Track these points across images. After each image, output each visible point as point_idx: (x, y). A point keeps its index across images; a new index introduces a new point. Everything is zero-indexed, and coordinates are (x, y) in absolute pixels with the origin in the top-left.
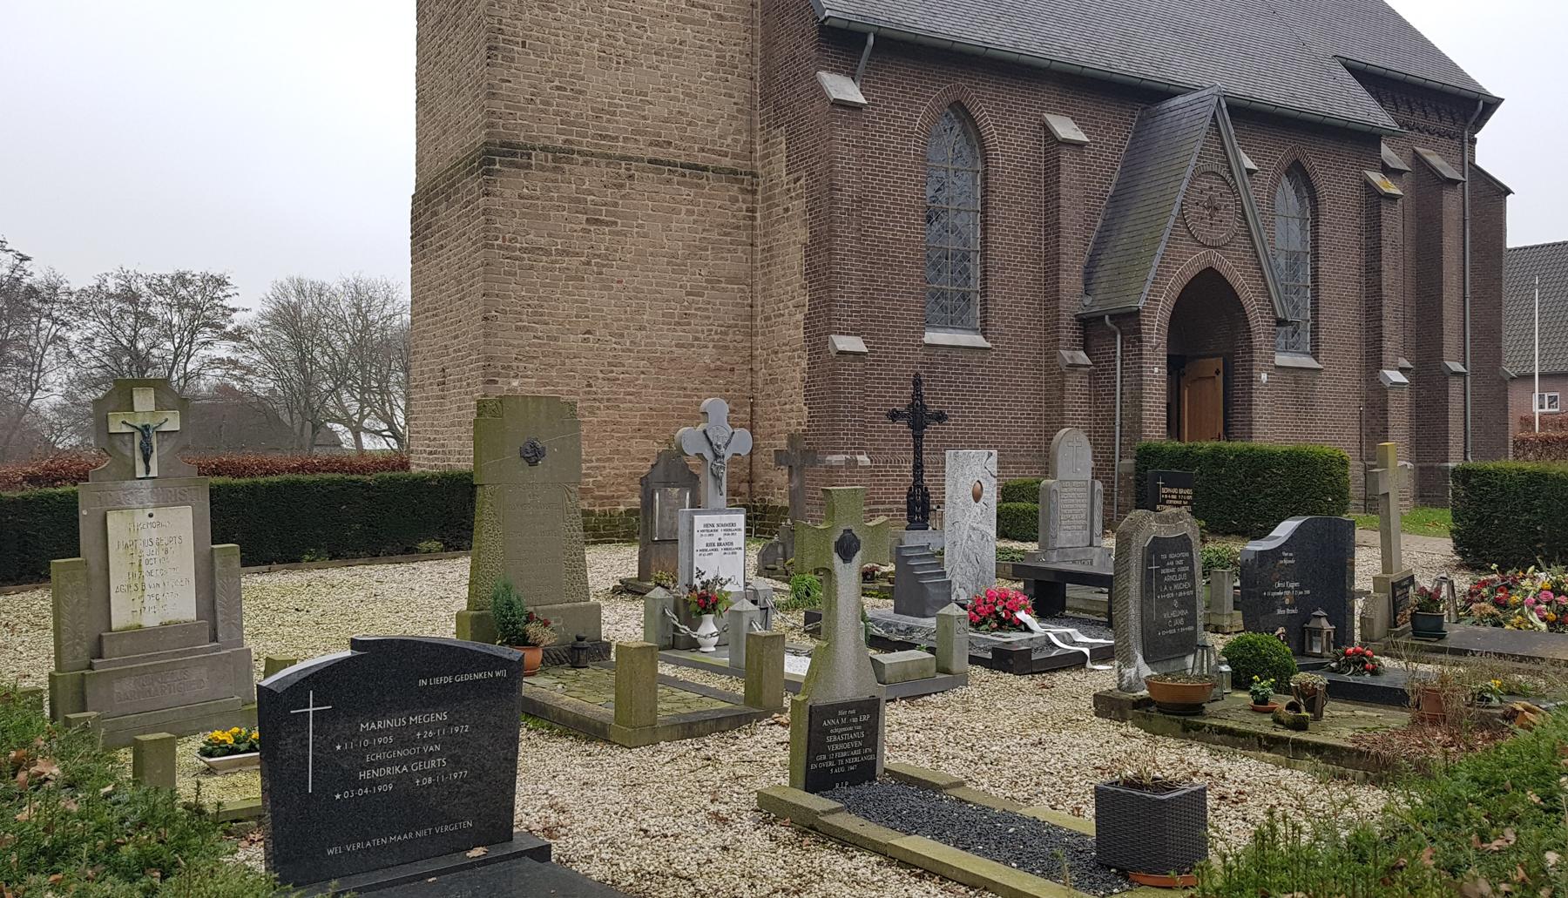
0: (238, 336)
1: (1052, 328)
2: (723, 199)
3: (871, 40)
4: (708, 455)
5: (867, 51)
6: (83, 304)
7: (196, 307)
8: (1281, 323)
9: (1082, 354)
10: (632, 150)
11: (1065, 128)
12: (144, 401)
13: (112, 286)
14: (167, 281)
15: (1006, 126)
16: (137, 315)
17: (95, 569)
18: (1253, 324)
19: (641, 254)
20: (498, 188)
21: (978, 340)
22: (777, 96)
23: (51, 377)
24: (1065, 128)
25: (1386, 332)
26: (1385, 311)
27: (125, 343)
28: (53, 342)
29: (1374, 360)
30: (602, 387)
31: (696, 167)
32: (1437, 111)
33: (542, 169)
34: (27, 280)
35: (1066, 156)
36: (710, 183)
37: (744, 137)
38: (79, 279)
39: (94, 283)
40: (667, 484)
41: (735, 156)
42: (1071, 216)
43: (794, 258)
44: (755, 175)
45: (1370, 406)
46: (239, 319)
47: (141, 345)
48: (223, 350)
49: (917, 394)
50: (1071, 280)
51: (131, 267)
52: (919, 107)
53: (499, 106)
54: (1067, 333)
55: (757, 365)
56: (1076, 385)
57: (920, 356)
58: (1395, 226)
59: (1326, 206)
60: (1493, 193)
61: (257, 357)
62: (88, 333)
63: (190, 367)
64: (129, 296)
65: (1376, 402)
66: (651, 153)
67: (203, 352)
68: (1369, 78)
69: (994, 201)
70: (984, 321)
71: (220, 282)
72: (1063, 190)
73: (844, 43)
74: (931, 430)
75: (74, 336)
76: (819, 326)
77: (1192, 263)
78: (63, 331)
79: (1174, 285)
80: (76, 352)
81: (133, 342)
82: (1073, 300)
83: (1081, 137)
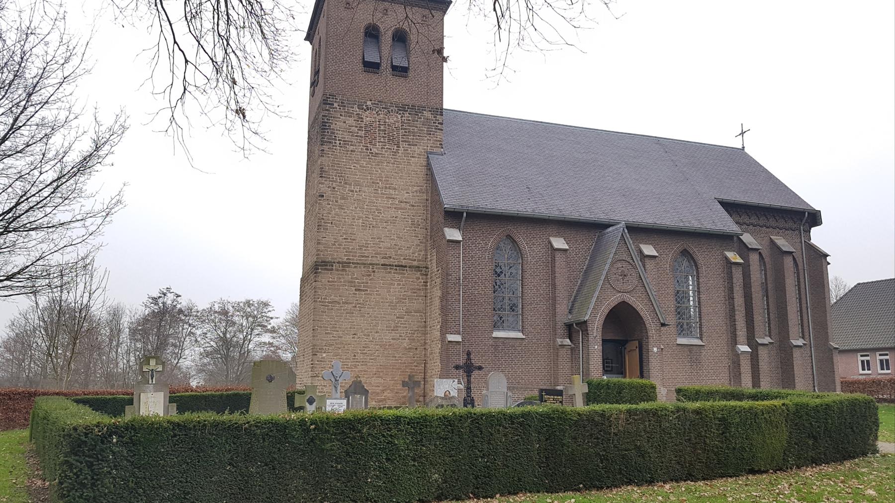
0: (273, 331)
1: (555, 329)
2: (413, 279)
3: (465, 214)
4: (333, 380)
5: (464, 219)
6: (204, 317)
7: (255, 317)
8: (663, 325)
9: (568, 340)
10: (375, 261)
11: (559, 243)
12: (153, 362)
13: (216, 308)
14: (241, 305)
15: (531, 245)
16: (227, 321)
17: (137, 409)
18: (648, 326)
19: (378, 302)
20: (319, 279)
21: (520, 335)
22: (434, 237)
23: (187, 352)
24: (559, 243)
25: (738, 327)
26: (737, 317)
27: (221, 335)
28: (189, 335)
29: (734, 342)
30: (360, 357)
31: (402, 266)
32: (783, 217)
33: (337, 270)
34: (179, 306)
35: (558, 255)
36: (408, 272)
37: (423, 253)
38: (202, 305)
39: (209, 306)
40: (355, 393)
41: (419, 261)
42: (561, 280)
43: (437, 302)
44: (427, 268)
45: (734, 363)
46: (274, 323)
47: (228, 336)
48: (266, 338)
49: (469, 359)
50: (562, 308)
51: (225, 298)
52: (489, 240)
53: (321, 247)
54: (561, 330)
55: (427, 347)
56: (564, 354)
57: (491, 342)
58: (738, 274)
59: (703, 269)
60: (819, 258)
61: (283, 341)
62: (205, 331)
63: (250, 346)
64: (224, 312)
65: (736, 359)
66: (382, 261)
67: (257, 339)
68: (730, 207)
69: (527, 275)
70: (701, 335)
71: (266, 304)
73: (454, 217)
74: (475, 373)
75: (199, 332)
76: (444, 331)
77: (613, 300)
78: (194, 330)
79: (604, 310)
80: (199, 339)
81: (225, 334)
82: (563, 315)
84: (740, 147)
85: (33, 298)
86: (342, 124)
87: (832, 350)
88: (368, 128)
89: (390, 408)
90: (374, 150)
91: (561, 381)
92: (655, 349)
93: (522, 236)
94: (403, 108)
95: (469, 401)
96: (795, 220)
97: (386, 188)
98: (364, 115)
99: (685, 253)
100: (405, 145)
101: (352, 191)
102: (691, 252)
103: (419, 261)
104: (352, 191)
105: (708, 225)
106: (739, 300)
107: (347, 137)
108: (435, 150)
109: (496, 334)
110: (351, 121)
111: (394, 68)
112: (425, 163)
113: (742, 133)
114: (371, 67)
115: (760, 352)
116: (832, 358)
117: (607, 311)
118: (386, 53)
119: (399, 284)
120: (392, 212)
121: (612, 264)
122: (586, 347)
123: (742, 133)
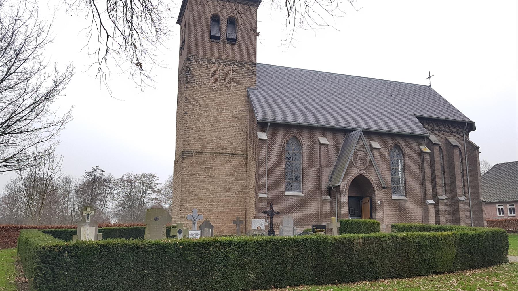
0: (158, 191)
1: (321, 191)
2: (239, 161)
3: (269, 124)
4: (193, 220)
5: (268, 127)
6: (118, 183)
7: (147, 183)
8: (384, 188)
9: (329, 197)
10: (217, 151)
11: (323, 141)
12: (88, 210)
13: (125, 178)
14: (140, 176)
15: (307, 142)
16: (131, 186)
17: (79, 236)
18: (375, 188)
20: (185, 161)
21: (301, 194)
22: (251, 137)
23: (108, 204)
24: (323, 141)
25: (427, 189)
26: (426, 183)
27: (128, 194)
28: (109, 194)
29: (425, 198)
30: (208, 206)
31: (233, 154)
33: (195, 156)
34: (103, 177)
35: (323, 148)
36: (236, 158)
37: (245, 146)
38: (117, 176)
39: (121, 177)
40: (206, 228)
41: (242, 151)
42: (325, 162)
43: (253, 175)
44: (247, 155)
45: (425, 210)
46: (158, 187)
47: (132, 194)
48: (154, 196)
49: (271, 207)
50: (325, 178)
51: (130, 173)
52: (283, 139)
53: (186, 143)
54: (325, 191)
55: (247, 201)
56: (327, 205)
57: (284, 198)
58: (427, 159)
59: (407, 156)
60: (474, 149)
61: (164, 197)
62: (119, 191)
63: (145, 200)
64: (130, 181)
65: (426, 208)
66: (221, 151)
67: (149, 196)
68: (423, 120)
69: (305, 159)
70: (406, 194)
71: (154, 176)
72: (322, 156)
73: (263, 125)
74: (275, 216)
75: (115, 192)
76: (257, 192)
77: (355, 173)
78: (112, 191)
79: (350, 179)
80: (115, 196)
81: (130, 193)
82: (326, 182)
83: (379, 146)
84: (429, 85)
85: (19, 172)
86: (198, 72)
87: (481, 202)
88: (213, 74)
89: (226, 236)
90: (217, 87)
91: (324, 220)
92: (379, 202)
93: (302, 137)
94: (233, 63)
95: (271, 232)
96: (460, 127)
97: (223, 109)
98: (211, 66)
99: (397, 146)
100: (235, 84)
101: (204, 111)
102: (400, 146)
103: (242, 151)
104: (204, 111)
105: (410, 130)
106: (428, 174)
107: (201, 79)
108: (252, 87)
109: (287, 193)
110: (203, 70)
111: (228, 39)
112: (246, 94)
113: (430, 77)
114: (215, 39)
115: (440, 204)
116: (482, 207)
117: (351, 180)
118: (224, 31)
119: (231, 165)
120: (227, 123)
121: (354, 153)
122: (339, 201)
123: (430, 77)
